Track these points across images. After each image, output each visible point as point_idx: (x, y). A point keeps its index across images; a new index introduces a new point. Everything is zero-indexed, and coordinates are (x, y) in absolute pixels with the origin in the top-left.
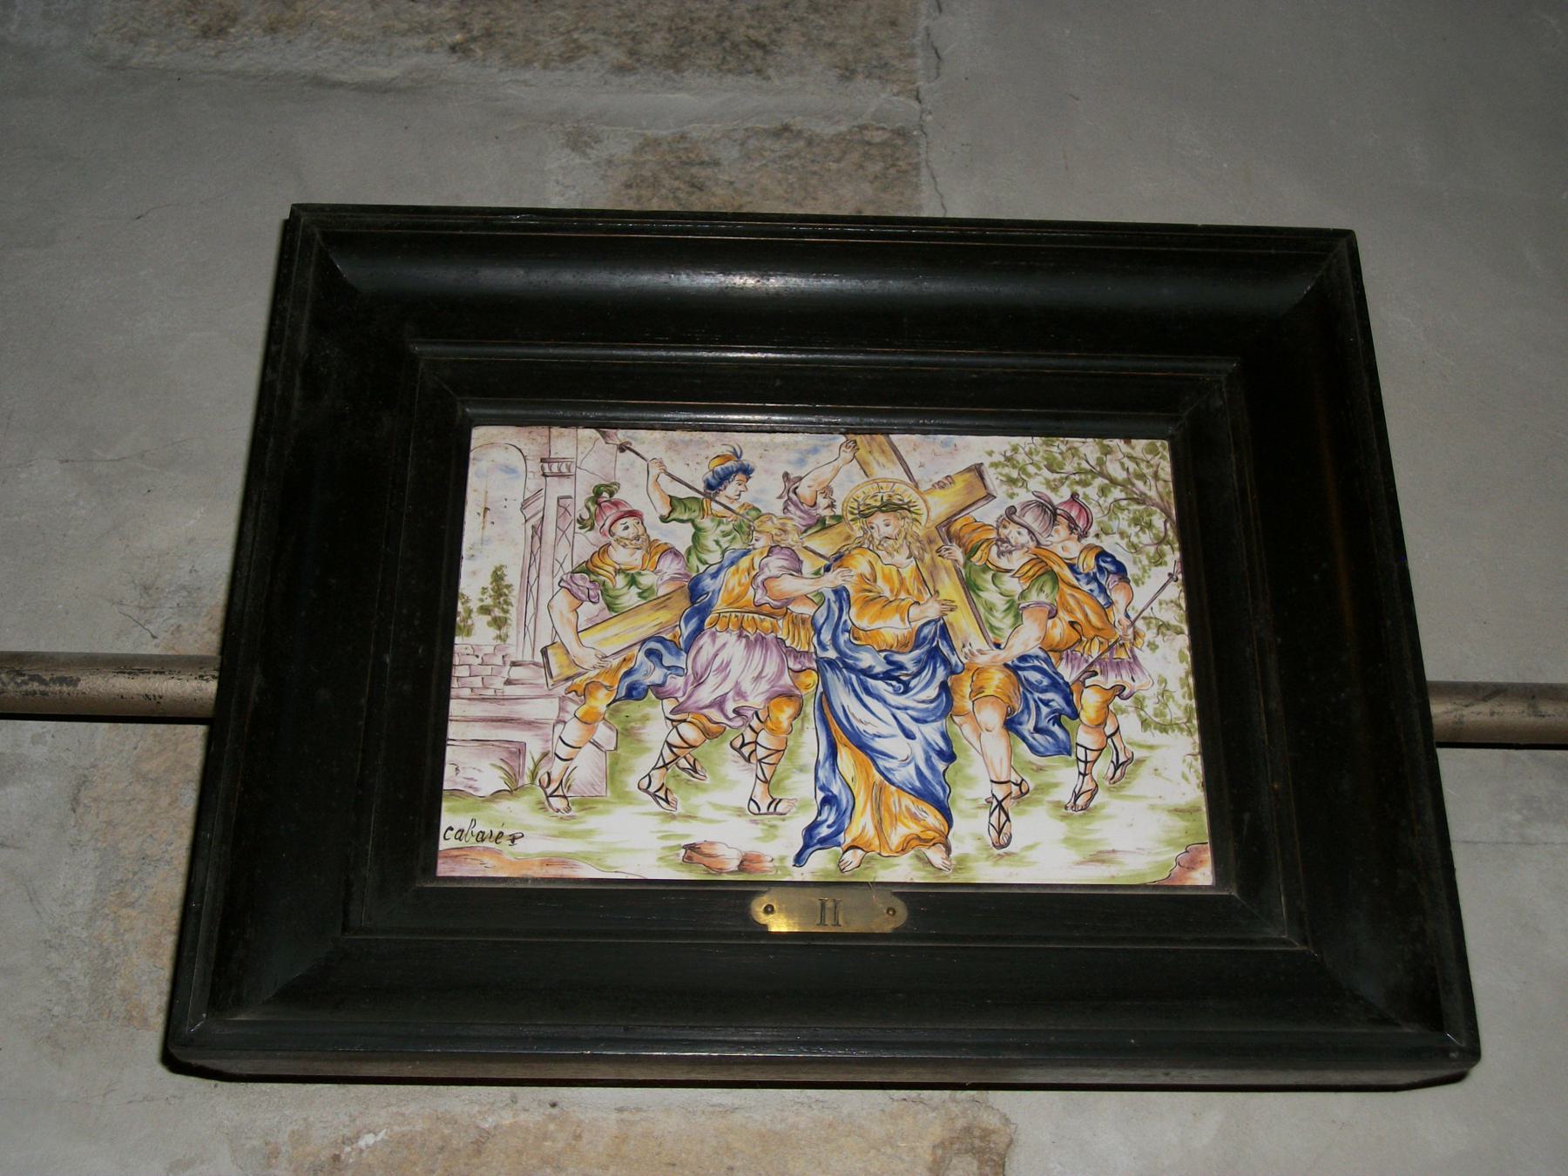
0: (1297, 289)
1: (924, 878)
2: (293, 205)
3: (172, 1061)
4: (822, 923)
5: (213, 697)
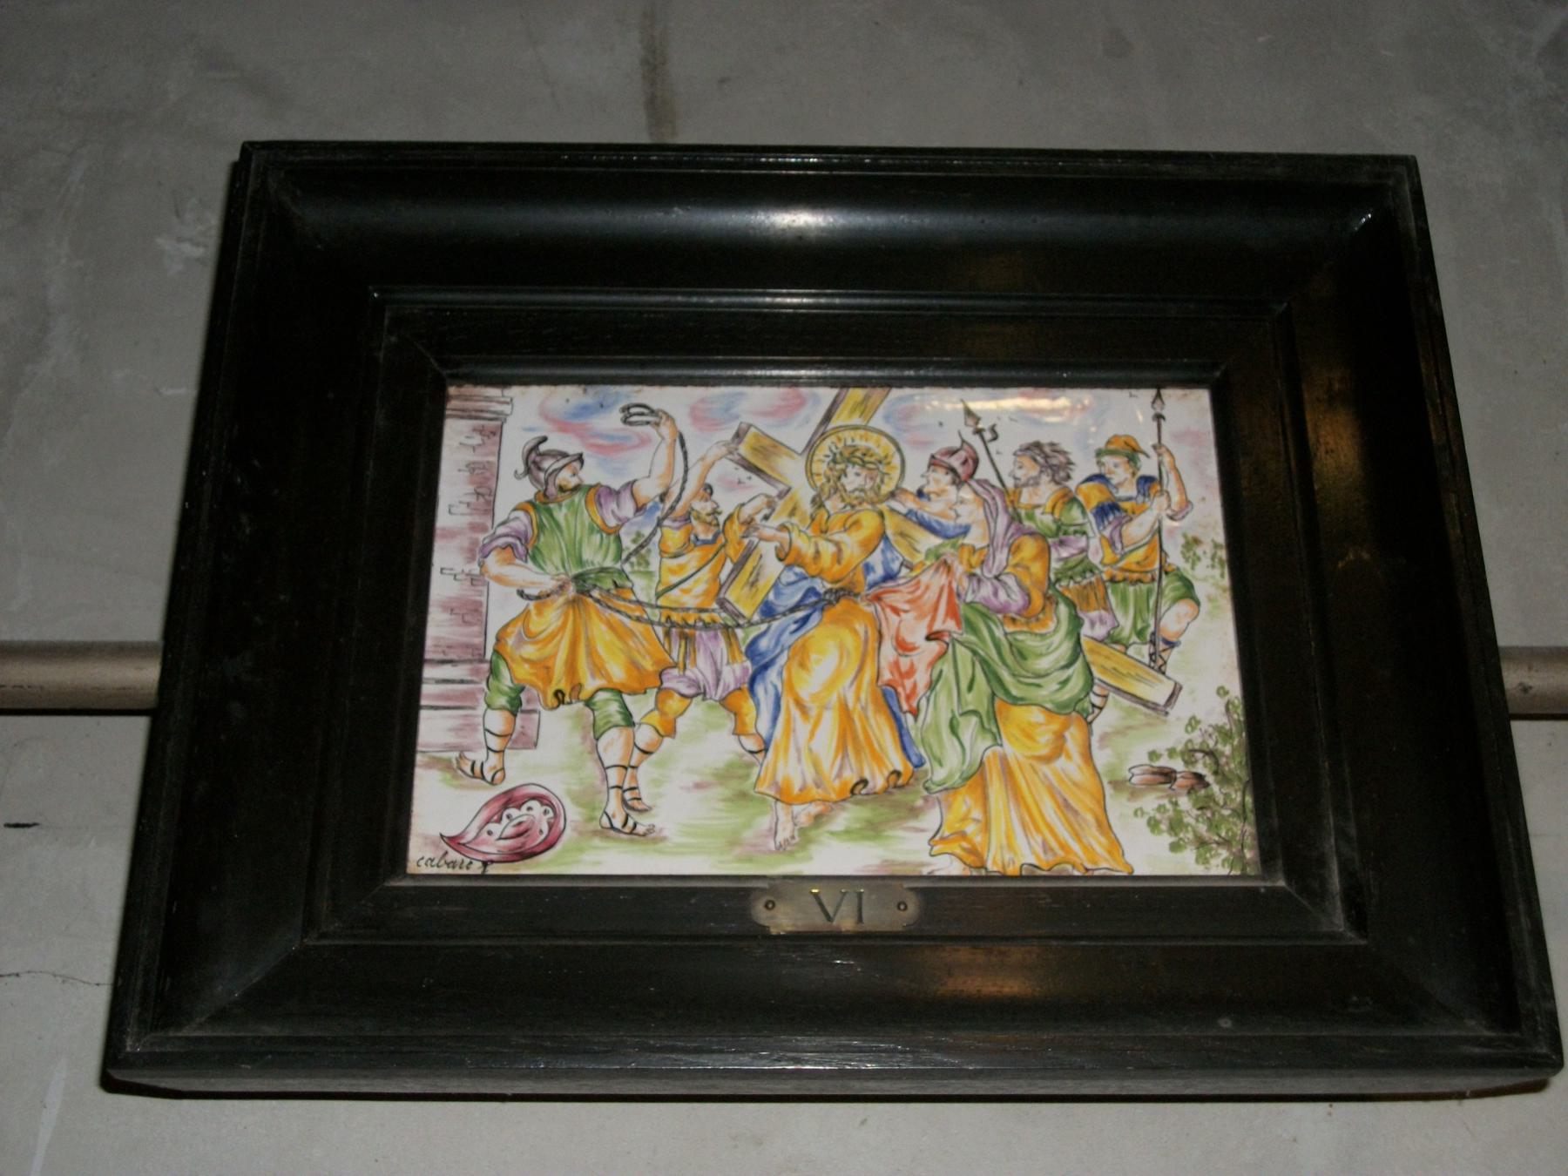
3: (109, 1084)
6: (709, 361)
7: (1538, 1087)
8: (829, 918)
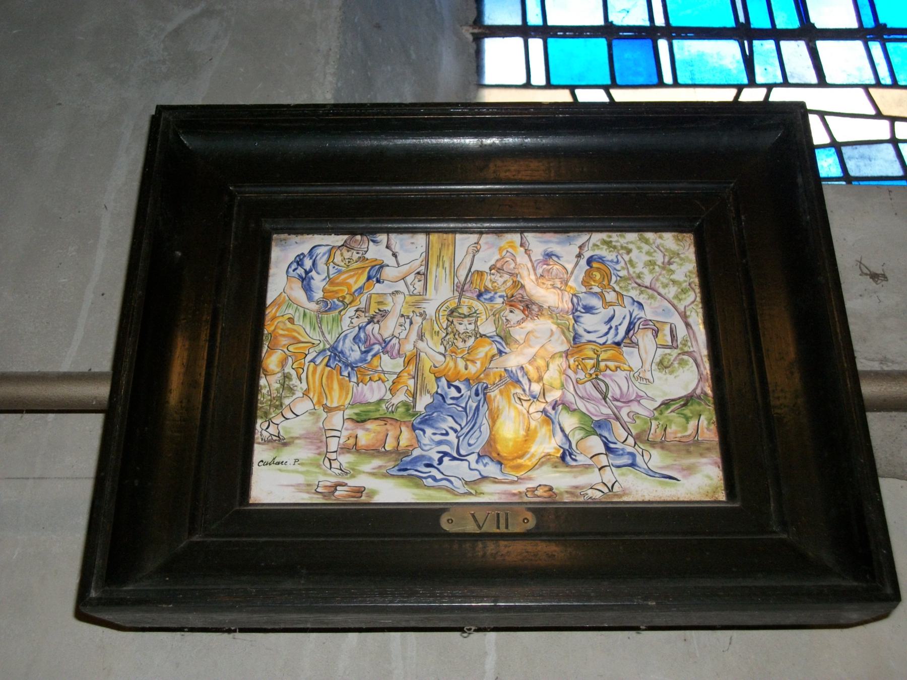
0: (768, 139)
1: (418, 499)
2: (160, 109)
3: (81, 615)
4: (498, 527)
5: (861, 381)
6: (409, 219)
7: (885, 616)
8: (480, 527)
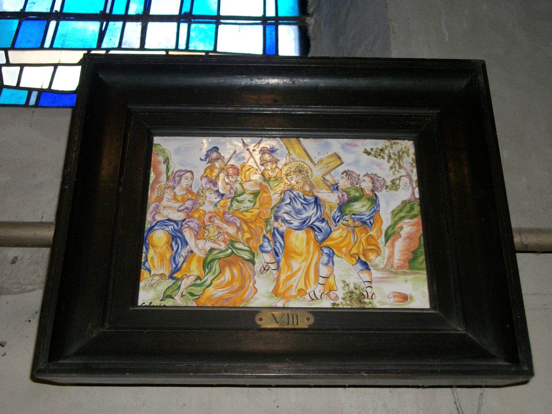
0: (463, 83)
